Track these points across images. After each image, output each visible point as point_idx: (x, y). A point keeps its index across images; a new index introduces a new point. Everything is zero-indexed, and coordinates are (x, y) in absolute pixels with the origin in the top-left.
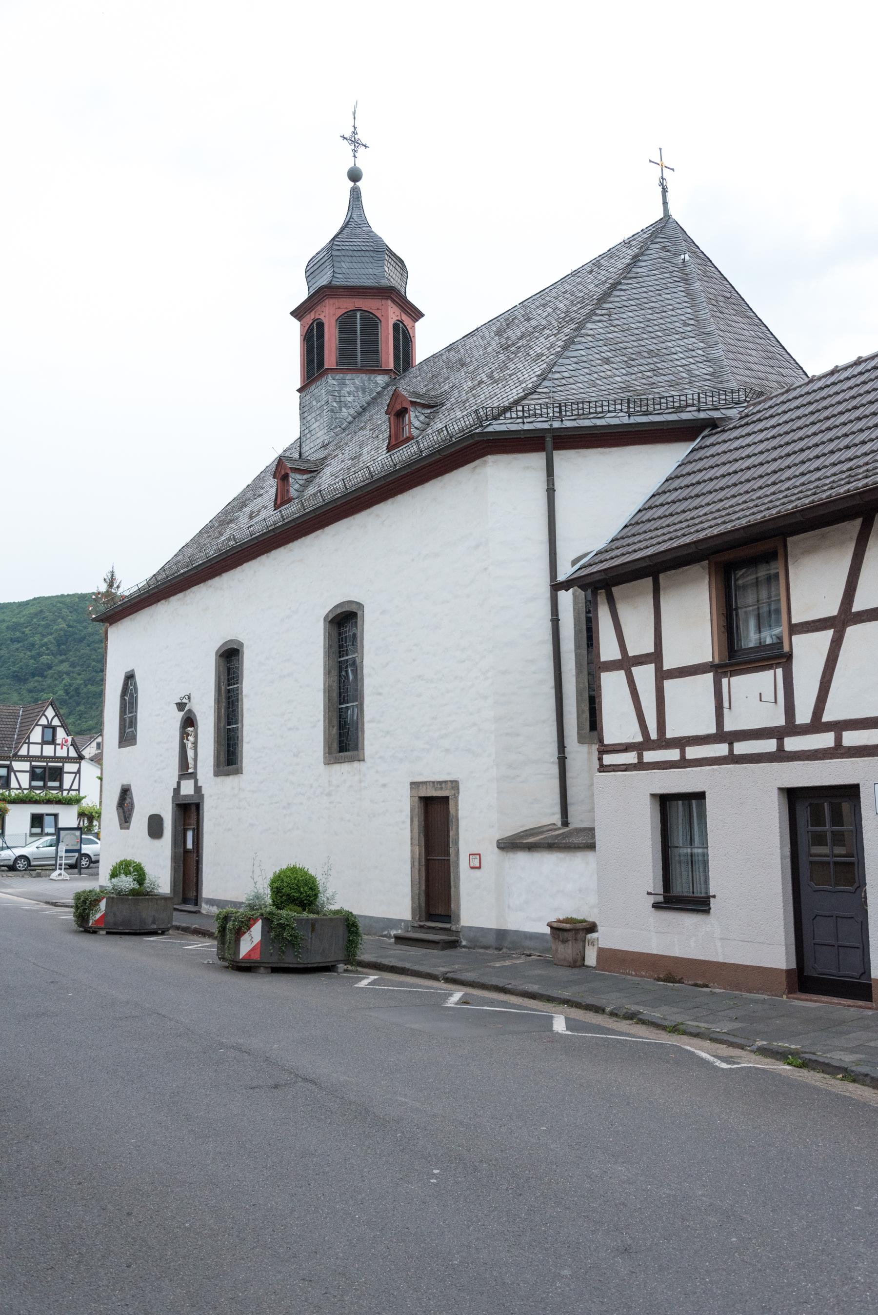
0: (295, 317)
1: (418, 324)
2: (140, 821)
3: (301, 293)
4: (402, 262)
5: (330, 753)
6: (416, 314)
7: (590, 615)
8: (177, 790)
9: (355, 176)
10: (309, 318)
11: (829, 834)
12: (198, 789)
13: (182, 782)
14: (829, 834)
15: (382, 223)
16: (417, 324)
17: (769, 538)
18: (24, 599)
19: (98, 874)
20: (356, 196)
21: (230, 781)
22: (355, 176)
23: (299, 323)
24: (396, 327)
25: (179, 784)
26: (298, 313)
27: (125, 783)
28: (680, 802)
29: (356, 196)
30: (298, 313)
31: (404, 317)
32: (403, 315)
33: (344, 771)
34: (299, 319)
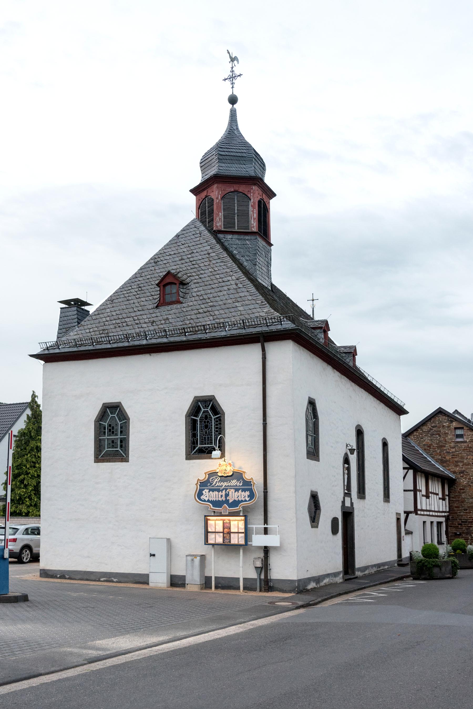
0: (193, 193)
1: (271, 201)
3: (197, 179)
4: (264, 165)
5: (359, 493)
6: (272, 195)
7: (346, 466)
9: (233, 100)
10: (203, 194)
11: (117, 437)
13: (346, 498)
14: (117, 437)
15: (251, 133)
17: (73, 667)
18: (9, 403)
22: (233, 100)
23: (195, 197)
31: (264, 196)
32: (264, 195)
34: (196, 195)
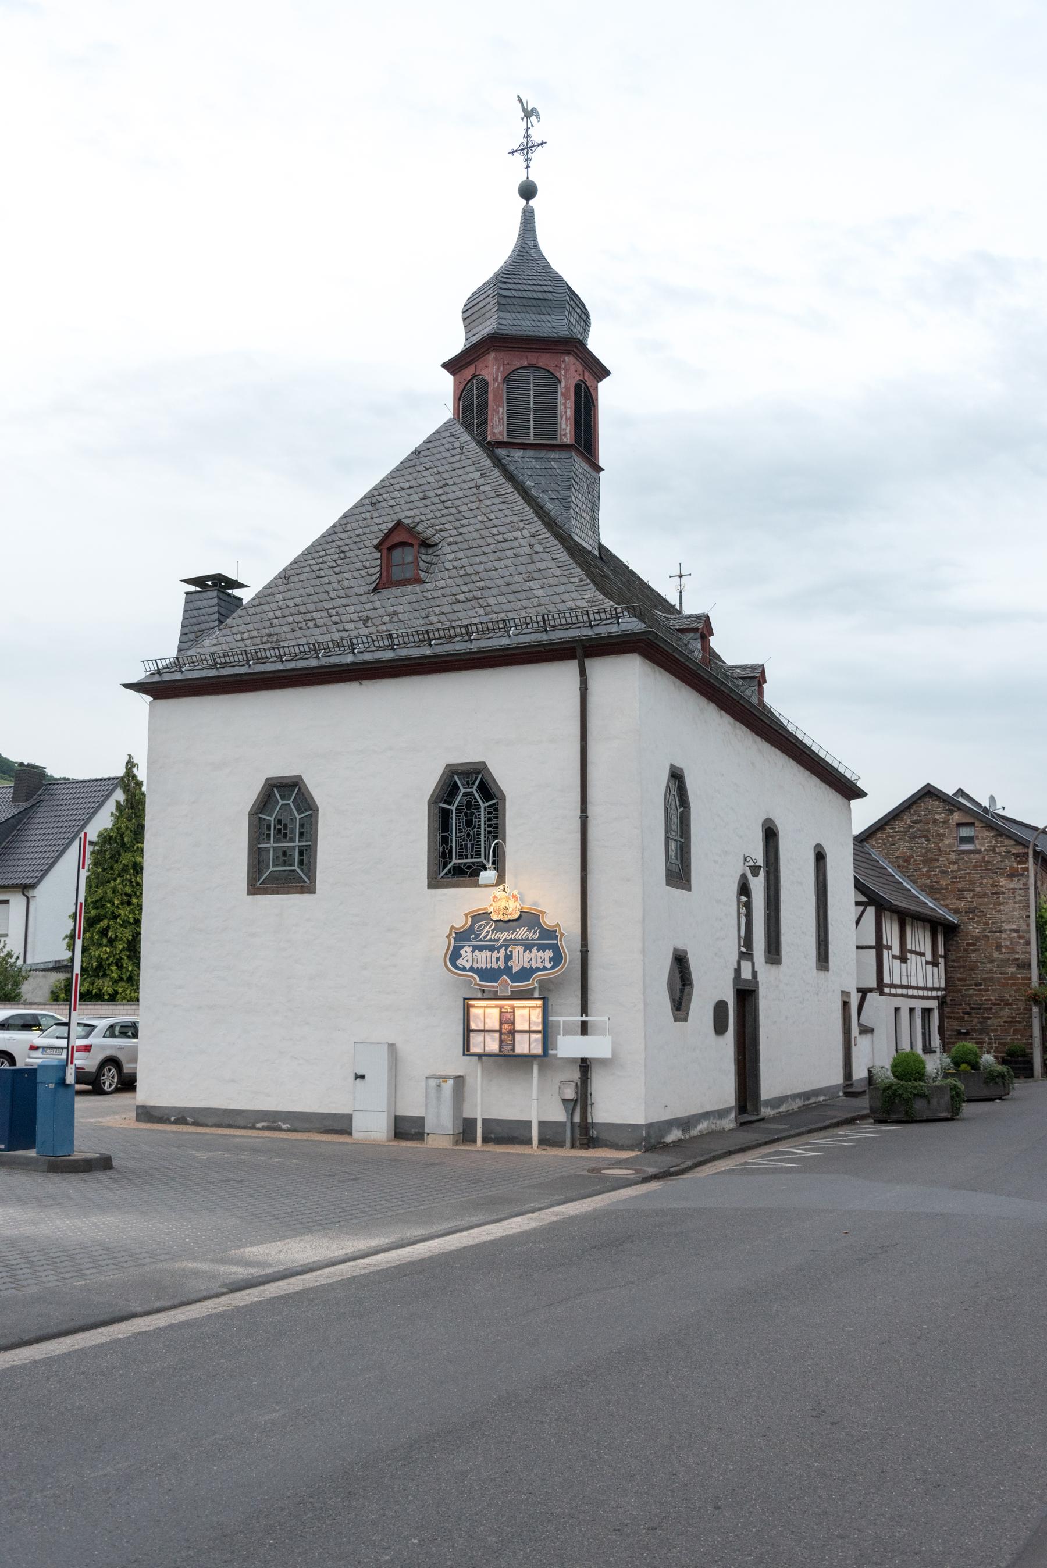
2: (701, 1008)
3: (456, 343)
6: (602, 372)
8: (738, 971)
9: (528, 191)
12: (754, 974)
13: (743, 962)
15: (560, 254)
16: (600, 384)
19: (138, 1000)
20: (528, 219)
21: (773, 968)
22: (528, 191)
23: (451, 378)
24: (578, 387)
25: (739, 963)
26: (452, 366)
27: (680, 946)
28: (551, 1019)
29: (528, 219)
30: (452, 366)
32: (587, 374)
33: (822, 974)
